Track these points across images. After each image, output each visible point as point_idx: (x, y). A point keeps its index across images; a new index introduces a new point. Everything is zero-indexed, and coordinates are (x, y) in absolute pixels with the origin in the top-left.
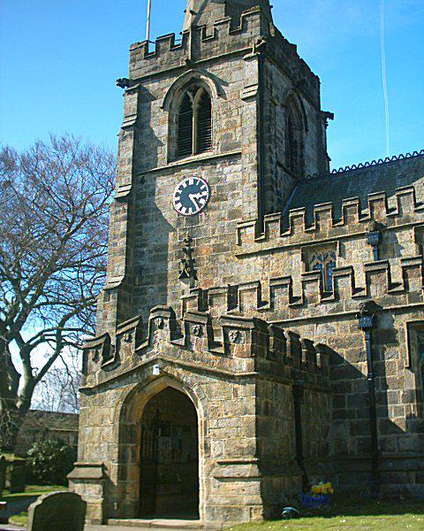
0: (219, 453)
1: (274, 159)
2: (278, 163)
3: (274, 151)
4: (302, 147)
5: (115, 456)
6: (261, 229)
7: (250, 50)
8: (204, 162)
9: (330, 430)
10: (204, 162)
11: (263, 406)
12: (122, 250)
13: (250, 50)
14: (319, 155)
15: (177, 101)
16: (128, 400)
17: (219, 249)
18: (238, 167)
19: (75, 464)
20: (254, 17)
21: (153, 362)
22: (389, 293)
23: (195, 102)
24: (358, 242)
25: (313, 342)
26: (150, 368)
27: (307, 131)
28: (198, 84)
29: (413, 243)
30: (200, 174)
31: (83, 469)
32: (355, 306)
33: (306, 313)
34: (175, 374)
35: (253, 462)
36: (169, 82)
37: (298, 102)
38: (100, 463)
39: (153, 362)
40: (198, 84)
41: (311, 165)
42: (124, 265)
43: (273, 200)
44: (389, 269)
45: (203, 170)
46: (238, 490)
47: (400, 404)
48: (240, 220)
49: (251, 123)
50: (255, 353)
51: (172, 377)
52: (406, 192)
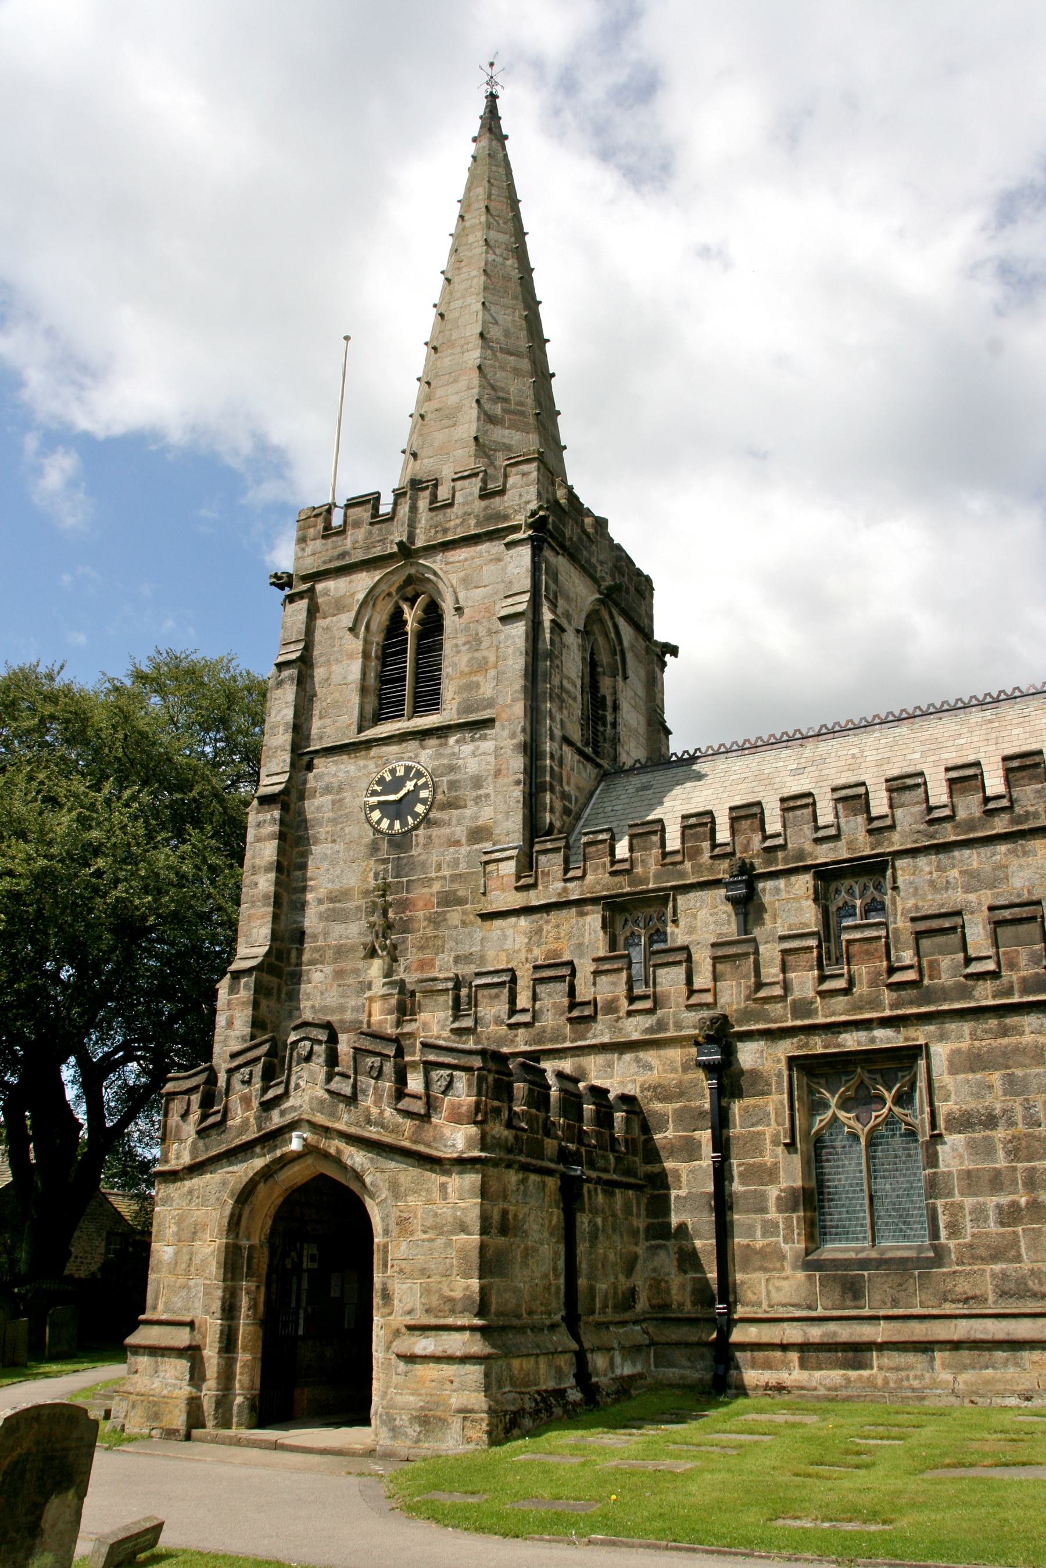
0: (408, 1308)
1: (558, 733)
2: (566, 740)
3: (558, 717)
4: (616, 708)
5: (216, 1305)
6: (527, 863)
7: (516, 529)
8: (423, 735)
9: (640, 1262)
10: (423, 735)
11: (496, 1216)
12: (266, 897)
13: (516, 529)
14: (649, 723)
15: (380, 618)
16: (245, 1195)
17: (449, 900)
18: (487, 746)
19: (142, 1317)
20: (525, 468)
21: (293, 1126)
22: (755, 1000)
23: (411, 616)
24: (707, 895)
25: (608, 1091)
26: (287, 1136)
27: (625, 678)
28: (420, 588)
29: (810, 902)
30: (417, 756)
31: (156, 1330)
32: (691, 1023)
33: (601, 1033)
34: (332, 1151)
35: (472, 1329)
36: (363, 582)
37: (610, 624)
38: (188, 1319)
39: (293, 1126)
40: (420, 588)
41: (632, 744)
42: (270, 926)
43: (552, 811)
44: (756, 952)
45: (423, 747)
46: (442, 1382)
47: (773, 1215)
48: (488, 846)
49: (516, 664)
50: (480, 1116)
51: (326, 1155)
52: (799, 803)
